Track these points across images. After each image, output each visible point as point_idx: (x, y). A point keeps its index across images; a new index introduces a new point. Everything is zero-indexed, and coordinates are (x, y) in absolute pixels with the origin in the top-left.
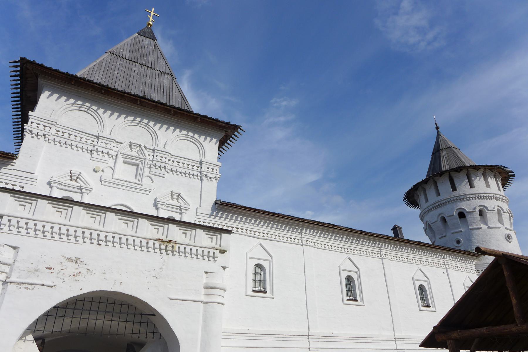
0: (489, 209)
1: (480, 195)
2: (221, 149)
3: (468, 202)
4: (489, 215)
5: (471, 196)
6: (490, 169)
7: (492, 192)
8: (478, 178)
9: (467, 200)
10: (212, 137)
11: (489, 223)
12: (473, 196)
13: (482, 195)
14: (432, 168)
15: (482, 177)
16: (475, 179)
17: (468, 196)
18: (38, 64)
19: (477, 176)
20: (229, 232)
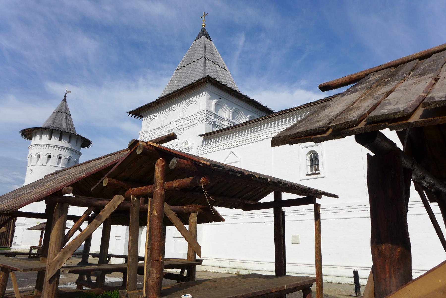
10: (230, 107)
18: (247, 97)
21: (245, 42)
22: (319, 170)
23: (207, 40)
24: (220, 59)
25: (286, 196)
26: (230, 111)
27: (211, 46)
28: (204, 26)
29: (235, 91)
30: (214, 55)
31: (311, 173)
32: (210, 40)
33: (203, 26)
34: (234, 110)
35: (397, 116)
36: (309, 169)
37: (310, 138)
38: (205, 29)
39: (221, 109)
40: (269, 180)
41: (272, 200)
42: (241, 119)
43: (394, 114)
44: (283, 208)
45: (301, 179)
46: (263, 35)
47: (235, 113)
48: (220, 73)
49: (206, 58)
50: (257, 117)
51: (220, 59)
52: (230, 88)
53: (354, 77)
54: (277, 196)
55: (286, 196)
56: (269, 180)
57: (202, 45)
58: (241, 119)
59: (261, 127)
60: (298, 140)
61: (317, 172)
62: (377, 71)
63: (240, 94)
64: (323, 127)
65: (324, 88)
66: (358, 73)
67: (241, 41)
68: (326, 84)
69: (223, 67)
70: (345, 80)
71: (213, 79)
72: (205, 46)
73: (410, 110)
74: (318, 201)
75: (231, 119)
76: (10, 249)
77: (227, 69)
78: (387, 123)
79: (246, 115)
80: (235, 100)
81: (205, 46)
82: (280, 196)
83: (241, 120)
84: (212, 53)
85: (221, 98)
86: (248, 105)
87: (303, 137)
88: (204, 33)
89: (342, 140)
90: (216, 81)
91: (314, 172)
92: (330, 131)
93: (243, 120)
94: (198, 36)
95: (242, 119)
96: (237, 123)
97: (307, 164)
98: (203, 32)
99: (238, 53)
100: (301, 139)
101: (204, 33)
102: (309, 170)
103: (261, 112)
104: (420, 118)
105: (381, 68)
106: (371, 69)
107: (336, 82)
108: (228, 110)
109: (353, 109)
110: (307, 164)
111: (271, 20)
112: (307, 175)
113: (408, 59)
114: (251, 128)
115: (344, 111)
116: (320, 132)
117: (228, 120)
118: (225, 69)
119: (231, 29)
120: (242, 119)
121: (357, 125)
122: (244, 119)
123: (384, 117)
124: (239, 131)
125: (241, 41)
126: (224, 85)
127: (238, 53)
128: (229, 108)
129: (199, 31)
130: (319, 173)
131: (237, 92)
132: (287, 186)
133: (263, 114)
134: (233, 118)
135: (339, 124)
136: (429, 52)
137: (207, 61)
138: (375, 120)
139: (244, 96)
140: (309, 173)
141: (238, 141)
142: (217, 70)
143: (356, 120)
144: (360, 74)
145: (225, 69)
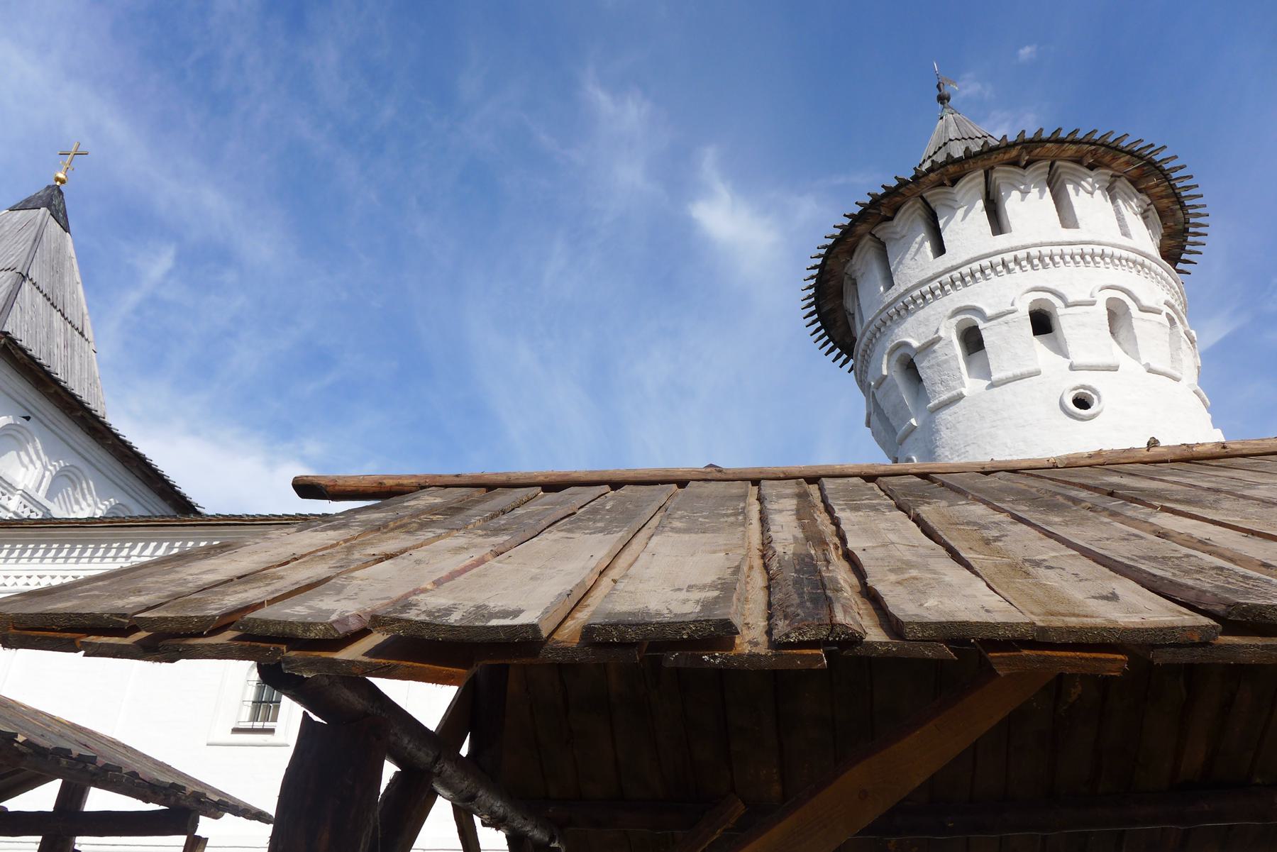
0: (989, 312)
1: (956, 274)
2: (1180, 266)
3: (921, 314)
4: (1065, 319)
5: (926, 288)
6: (1015, 163)
7: (1096, 239)
8: (960, 213)
9: (918, 308)
10: (51, 454)
11: (1071, 349)
12: (935, 284)
13: (965, 270)
14: (70, 400)
15: (1048, 189)
16: (946, 223)
17: (916, 293)
18: (124, 442)
19: (954, 210)
20: (236, 730)
21: (169, 274)
22: (275, 720)
23: (54, 227)
24: (77, 296)
25: (99, 800)
26: (45, 468)
27: (60, 249)
28: (63, 182)
29: (89, 411)
30: (62, 277)
31: (249, 725)
32: (66, 229)
33: (57, 179)
34: (62, 469)
35: (312, 635)
36: (247, 711)
37: (72, 641)
38: (60, 193)
39: (14, 453)
40: (21, 739)
41: (49, 807)
42: (77, 502)
43: (307, 626)
44: (79, 839)
45: (211, 741)
46: (230, 276)
47: (64, 480)
48: (60, 340)
49: (24, 277)
50: (137, 511)
51: (77, 296)
52: (73, 396)
53: (389, 483)
54: (71, 798)
55: (99, 800)
56: (21, 739)
57: (31, 233)
58: (77, 502)
59: (132, 548)
60: (33, 638)
61: (268, 725)
62: (446, 486)
63: (104, 424)
64: (124, 616)
65: (305, 488)
66: (400, 477)
67: (158, 265)
68: (316, 481)
69: (78, 324)
70: (365, 484)
71: (23, 350)
72: (37, 239)
73: (354, 625)
74: (205, 826)
75: (40, 496)
76: (731, 645)
77: (89, 333)
78: (284, 648)
79: (102, 496)
80: (80, 438)
81: (37, 239)
82: (81, 796)
83: (76, 508)
84: (57, 268)
85: (28, 418)
86: (118, 467)
87: (53, 630)
88: (52, 201)
89: (165, 666)
90: (32, 358)
91: (258, 725)
92: (142, 635)
93: (83, 511)
94: (28, 201)
95: (84, 504)
96: (58, 512)
97: (244, 694)
98: (51, 197)
99: (134, 297)
100: (44, 638)
101: (52, 201)
102: (244, 720)
103: (157, 499)
104: (365, 655)
105: (457, 481)
106: (434, 477)
107: (340, 482)
108: (38, 464)
109: (266, 577)
110: (244, 694)
111: (265, 247)
112: (236, 730)
113: (521, 481)
114: (97, 543)
115: (239, 578)
116: (112, 629)
117: (26, 495)
118: (82, 334)
119: (135, 220)
120: (84, 504)
121: (213, 633)
122: (88, 506)
123: (280, 628)
124: (49, 543)
125: (158, 265)
126: (56, 382)
127: (134, 297)
128: (45, 459)
129: (35, 187)
130: (271, 731)
131: (96, 418)
132: (91, 767)
133: (160, 508)
134: (50, 495)
135: (166, 618)
136: (566, 478)
137: (27, 286)
138: (257, 631)
139: (116, 436)
140: (242, 726)
141: (35, 574)
142: (50, 325)
143: (214, 616)
144: (405, 482)
145: (82, 334)
